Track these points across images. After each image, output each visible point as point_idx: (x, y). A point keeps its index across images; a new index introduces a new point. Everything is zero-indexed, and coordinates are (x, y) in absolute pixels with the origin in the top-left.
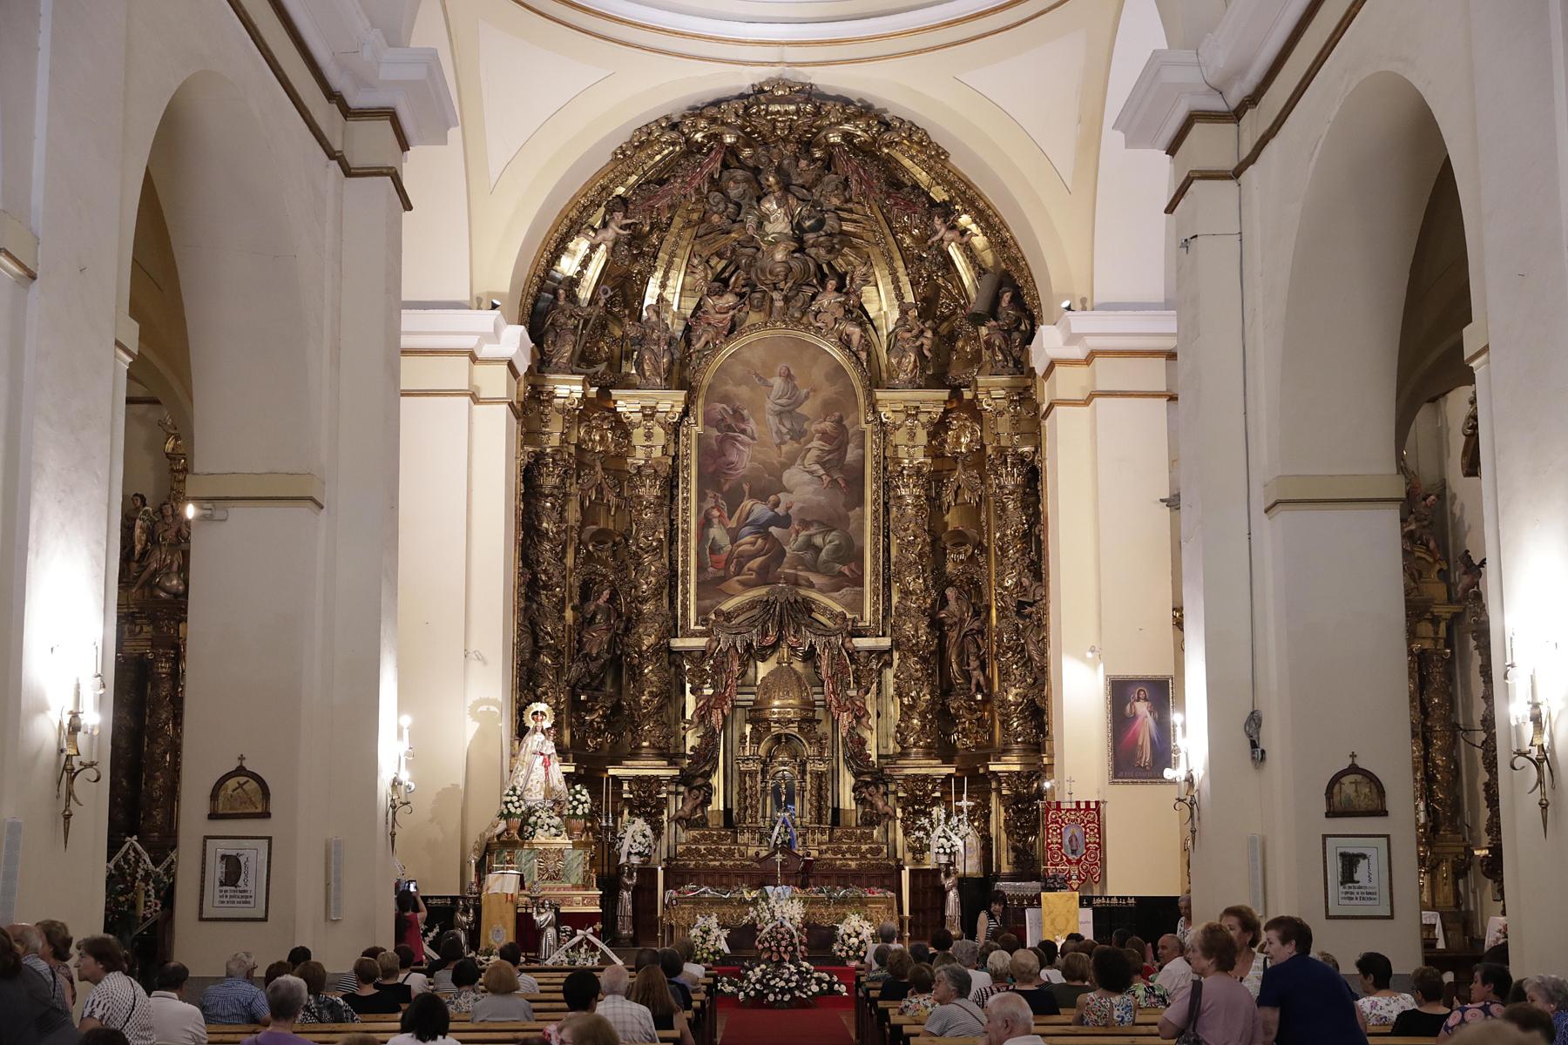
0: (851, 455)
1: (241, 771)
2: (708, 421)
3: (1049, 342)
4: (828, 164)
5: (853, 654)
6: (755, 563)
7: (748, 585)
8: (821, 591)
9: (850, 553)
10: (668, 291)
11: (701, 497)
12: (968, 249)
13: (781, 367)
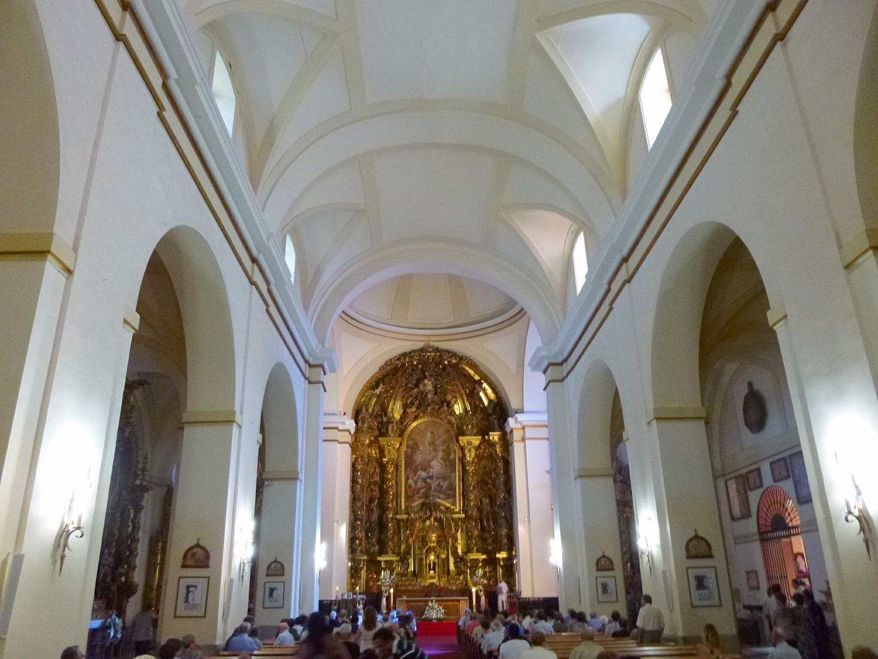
0: (452, 456)
1: (276, 561)
2: (407, 447)
3: (511, 422)
4: (444, 368)
5: (453, 519)
6: (423, 491)
7: (420, 498)
8: (443, 499)
9: (452, 488)
10: (396, 410)
11: (406, 471)
12: (486, 395)
13: (430, 429)
